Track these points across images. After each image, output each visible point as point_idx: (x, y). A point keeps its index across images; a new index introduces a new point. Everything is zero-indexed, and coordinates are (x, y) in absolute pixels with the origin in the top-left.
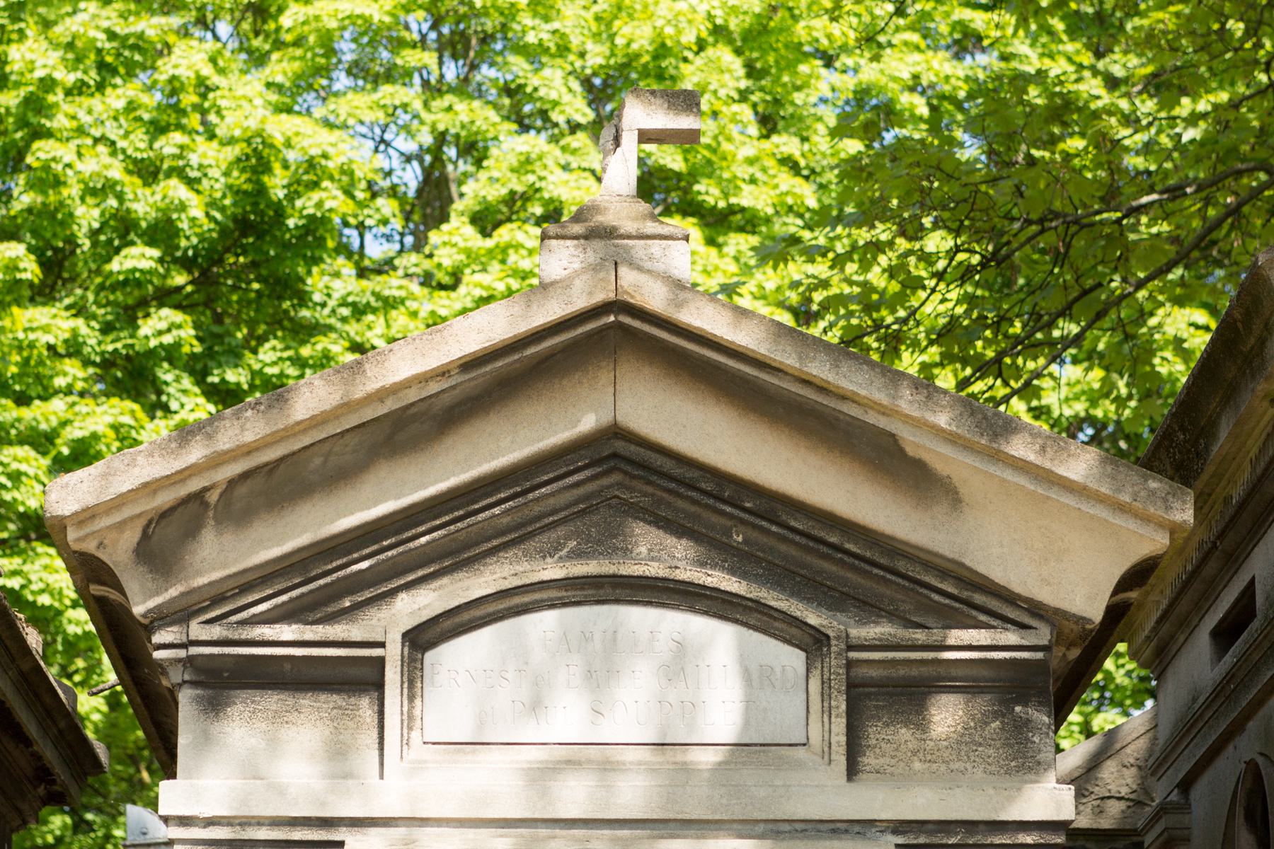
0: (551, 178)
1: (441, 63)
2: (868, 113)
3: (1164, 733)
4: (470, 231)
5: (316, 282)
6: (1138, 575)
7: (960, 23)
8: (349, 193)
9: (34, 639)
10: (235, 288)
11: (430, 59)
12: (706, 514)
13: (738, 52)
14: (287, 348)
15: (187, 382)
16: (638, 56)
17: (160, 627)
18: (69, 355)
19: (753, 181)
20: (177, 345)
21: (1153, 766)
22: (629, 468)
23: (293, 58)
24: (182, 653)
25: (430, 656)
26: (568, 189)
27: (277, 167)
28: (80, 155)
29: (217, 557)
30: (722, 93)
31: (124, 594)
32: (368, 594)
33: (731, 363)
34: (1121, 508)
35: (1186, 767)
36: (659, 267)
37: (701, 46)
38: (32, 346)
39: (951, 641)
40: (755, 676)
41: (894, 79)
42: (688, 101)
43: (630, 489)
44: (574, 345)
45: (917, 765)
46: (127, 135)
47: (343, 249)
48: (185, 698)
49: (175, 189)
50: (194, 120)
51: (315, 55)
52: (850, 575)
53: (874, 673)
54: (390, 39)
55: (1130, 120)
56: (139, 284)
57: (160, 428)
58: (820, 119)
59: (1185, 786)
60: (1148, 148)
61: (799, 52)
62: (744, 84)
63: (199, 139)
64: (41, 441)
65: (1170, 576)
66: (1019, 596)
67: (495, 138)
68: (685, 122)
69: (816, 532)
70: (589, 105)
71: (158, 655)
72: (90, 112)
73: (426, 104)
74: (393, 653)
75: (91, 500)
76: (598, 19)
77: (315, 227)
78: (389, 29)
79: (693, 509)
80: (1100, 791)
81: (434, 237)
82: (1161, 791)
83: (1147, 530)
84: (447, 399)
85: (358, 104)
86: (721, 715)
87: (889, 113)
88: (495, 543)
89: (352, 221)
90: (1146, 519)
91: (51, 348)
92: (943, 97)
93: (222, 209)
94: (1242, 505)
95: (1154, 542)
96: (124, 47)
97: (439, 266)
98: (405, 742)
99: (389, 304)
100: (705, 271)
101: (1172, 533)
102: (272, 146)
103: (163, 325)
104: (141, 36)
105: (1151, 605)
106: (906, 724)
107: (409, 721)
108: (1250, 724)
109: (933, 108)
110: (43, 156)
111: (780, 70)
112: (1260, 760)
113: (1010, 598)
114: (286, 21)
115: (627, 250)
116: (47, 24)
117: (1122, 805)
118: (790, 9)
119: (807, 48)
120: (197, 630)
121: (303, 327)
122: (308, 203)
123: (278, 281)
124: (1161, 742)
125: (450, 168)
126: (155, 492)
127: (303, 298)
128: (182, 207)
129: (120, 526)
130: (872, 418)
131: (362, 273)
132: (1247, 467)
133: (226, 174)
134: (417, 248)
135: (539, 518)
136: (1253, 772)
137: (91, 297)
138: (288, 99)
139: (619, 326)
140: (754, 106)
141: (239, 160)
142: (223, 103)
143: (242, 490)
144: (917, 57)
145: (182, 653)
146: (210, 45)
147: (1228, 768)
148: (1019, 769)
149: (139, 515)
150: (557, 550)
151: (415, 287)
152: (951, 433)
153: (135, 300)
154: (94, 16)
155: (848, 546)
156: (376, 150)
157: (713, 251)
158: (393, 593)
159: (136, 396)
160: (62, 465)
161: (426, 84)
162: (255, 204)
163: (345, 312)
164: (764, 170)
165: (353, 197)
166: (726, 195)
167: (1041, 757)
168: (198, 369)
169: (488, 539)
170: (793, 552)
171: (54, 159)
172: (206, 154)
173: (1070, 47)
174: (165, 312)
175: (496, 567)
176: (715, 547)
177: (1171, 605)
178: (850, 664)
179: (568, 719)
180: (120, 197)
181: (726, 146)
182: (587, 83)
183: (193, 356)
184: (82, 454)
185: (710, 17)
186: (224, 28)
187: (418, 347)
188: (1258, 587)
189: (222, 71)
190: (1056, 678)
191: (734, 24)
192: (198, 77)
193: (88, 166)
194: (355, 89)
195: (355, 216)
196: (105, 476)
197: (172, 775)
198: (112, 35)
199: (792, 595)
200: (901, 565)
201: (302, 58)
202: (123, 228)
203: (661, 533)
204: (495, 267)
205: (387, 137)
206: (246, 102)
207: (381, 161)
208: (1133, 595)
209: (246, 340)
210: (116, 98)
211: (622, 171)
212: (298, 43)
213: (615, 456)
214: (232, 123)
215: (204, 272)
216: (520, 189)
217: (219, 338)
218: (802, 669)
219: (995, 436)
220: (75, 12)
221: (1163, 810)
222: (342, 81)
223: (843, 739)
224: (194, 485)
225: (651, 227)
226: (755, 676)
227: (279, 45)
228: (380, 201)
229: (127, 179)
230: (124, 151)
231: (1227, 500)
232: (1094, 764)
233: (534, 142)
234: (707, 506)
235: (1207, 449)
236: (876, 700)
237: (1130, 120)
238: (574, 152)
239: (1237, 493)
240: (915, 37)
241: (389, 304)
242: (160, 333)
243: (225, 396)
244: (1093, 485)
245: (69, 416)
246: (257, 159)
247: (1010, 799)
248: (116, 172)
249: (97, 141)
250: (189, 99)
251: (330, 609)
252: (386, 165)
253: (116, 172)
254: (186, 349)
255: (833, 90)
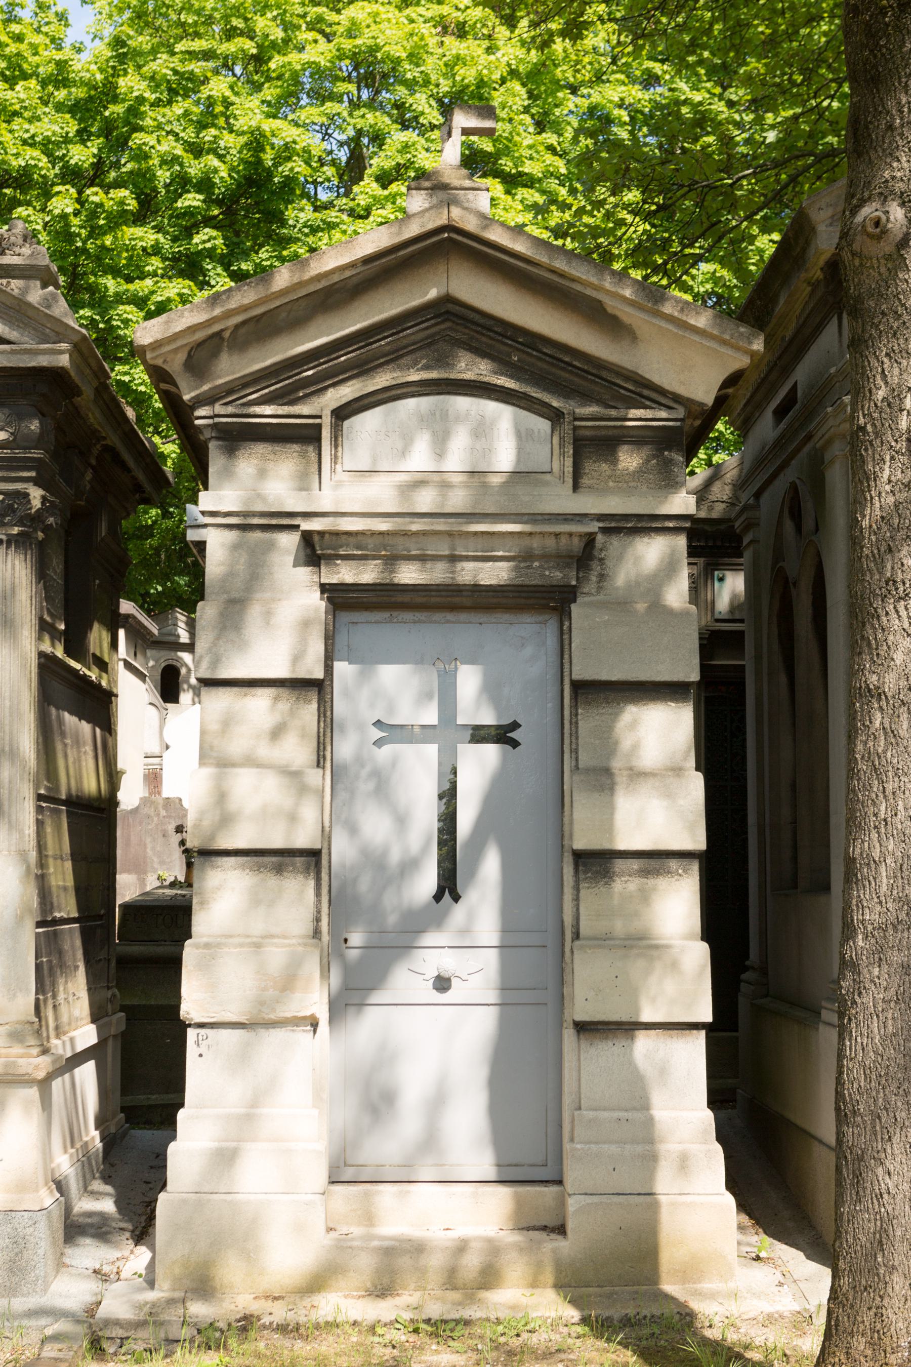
0: (419, 156)
1: (359, 90)
2: (598, 121)
3: (747, 465)
4: (375, 185)
5: (290, 214)
6: (733, 380)
7: (647, 69)
8: (307, 163)
9: (130, 413)
10: (246, 217)
11: (352, 88)
12: (498, 345)
13: (524, 85)
14: (274, 251)
15: (219, 270)
16: (468, 86)
17: (198, 407)
18: (155, 255)
19: (531, 158)
20: (214, 248)
21: (739, 485)
22: (455, 319)
23: (276, 87)
24: (210, 421)
25: (346, 424)
26: (426, 161)
27: (268, 147)
28: (159, 141)
29: (230, 368)
30: (514, 108)
31: (178, 387)
32: (312, 389)
33: (512, 260)
34: (724, 342)
35: (759, 485)
36: (472, 206)
37: (503, 81)
38: (133, 248)
39: (630, 416)
40: (523, 435)
41: (611, 102)
42: (488, 112)
43: (456, 331)
44: (426, 249)
45: (611, 484)
46: (184, 130)
47: (305, 195)
48: (212, 445)
49: (212, 161)
50: (221, 121)
51: (289, 85)
52: (576, 379)
53: (588, 433)
54: (331, 76)
55: (739, 125)
56: (192, 215)
57: (201, 296)
58: (569, 123)
59: (757, 495)
60: (747, 142)
61: (557, 85)
62: (526, 103)
63: (225, 132)
64: (140, 302)
65: (752, 379)
66: (668, 391)
67: (389, 133)
68: (488, 124)
69: (557, 355)
70: (441, 114)
71: (197, 422)
72: (164, 116)
73: (351, 115)
74: (326, 422)
75: (159, 336)
76: (446, 65)
77: (289, 182)
78: (330, 70)
79: (490, 342)
80: (712, 498)
81: (356, 189)
82: (745, 497)
83: (738, 355)
84: (355, 280)
85: (311, 113)
86: (504, 457)
87: (607, 121)
88: (382, 360)
89: (310, 180)
90: (738, 349)
91: (144, 249)
92: (637, 111)
93: (238, 172)
94: (791, 341)
95: (741, 362)
96: (183, 79)
97: (358, 205)
98: (333, 471)
99: (331, 226)
100: (505, 209)
101: (752, 357)
102: (265, 136)
103: (206, 238)
104: (192, 72)
105: (742, 394)
106: (605, 461)
107: (335, 459)
108: (793, 462)
109: (632, 118)
110: (138, 142)
111: (547, 96)
112: (797, 481)
113: (662, 392)
114: (272, 65)
115: (455, 196)
116: (139, 67)
117: (723, 506)
118: (553, 60)
119: (562, 83)
120: (218, 409)
121: (283, 239)
122: (285, 169)
123: (269, 213)
124: (745, 471)
125: (365, 150)
126: (194, 332)
127: (283, 223)
128: (216, 171)
129: (176, 351)
130: (588, 292)
131: (316, 209)
132: (795, 321)
133: (240, 152)
134: (347, 195)
135: (405, 347)
136: (794, 487)
137: (166, 221)
138: (274, 110)
139: (449, 239)
140: (533, 116)
141: (247, 144)
142: (237, 112)
143: (242, 331)
144: (623, 88)
145: (210, 421)
146: (231, 79)
147: (780, 486)
148: (666, 486)
149: (186, 345)
150: (416, 365)
151: (345, 217)
152: (632, 300)
153: (189, 224)
154: (166, 61)
155: (575, 363)
156: (323, 140)
157: (509, 198)
158: (326, 388)
159: (192, 277)
160: (149, 316)
161: (351, 101)
162: (256, 169)
163: (306, 230)
164: (538, 152)
165: (310, 166)
166: (516, 167)
167: (678, 479)
168: (225, 262)
169: (378, 359)
170: (545, 366)
171: (144, 144)
172: (228, 140)
173: (709, 85)
174: (207, 230)
175: (394, 370)
176: (505, 365)
177: (752, 396)
178: (575, 428)
179: (420, 458)
180: (181, 165)
181: (517, 138)
182: (440, 101)
183: (222, 255)
184: (162, 308)
185: (509, 65)
186: (238, 70)
187: (344, 248)
188: (799, 386)
189: (237, 94)
190: (687, 436)
191: (521, 69)
192: (223, 97)
193: (163, 148)
194: (311, 105)
195: (312, 176)
196: (167, 322)
197: (206, 489)
198: (176, 72)
199: (544, 390)
200: (604, 374)
201: (281, 86)
202: (182, 183)
203: (473, 356)
204: (389, 206)
205: (330, 131)
206: (250, 112)
207: (325, 145)
208: (730, 391)
209: (253, 247)
210: (178, 109)
211: (453, 151)
212: (279, 78)
213: (448, 312)
214: (241, 123)
215: (229, 208)
216: (402, 162)
217: (237, 244)
218: (549, 431)
219: (656, 302)
220: (154, 60)
221: (745, 508)
222: (305, 100)
223: (571, 469)
224: (216, 328)
225: (467, 183)
226: (523, 435)
227: (269, 79)
228: (325, 168)
229: (185, 154)
230: (183, 138)
231: (783, 338)
232: (708, 484)
233: (410, 136)
234: (498, 341)
235: (773, 310)
236: (589, 448)
237: (739, 125)
238: (432, 141)
239: (789, 334)
240: (622, 77)
241: (331, 226)
242: (204, 242)
243: (239, 277)
244: (709, 330)
245: (155, 288)
246: (257, 142)
247: (662, 503)
248: (179, 151)
249: (168, 133)
250: (219, 109)
251: (292, 397)
252: (329, 148)
253: (179, 151)
254: (219, 251)
255: (576, 106)
